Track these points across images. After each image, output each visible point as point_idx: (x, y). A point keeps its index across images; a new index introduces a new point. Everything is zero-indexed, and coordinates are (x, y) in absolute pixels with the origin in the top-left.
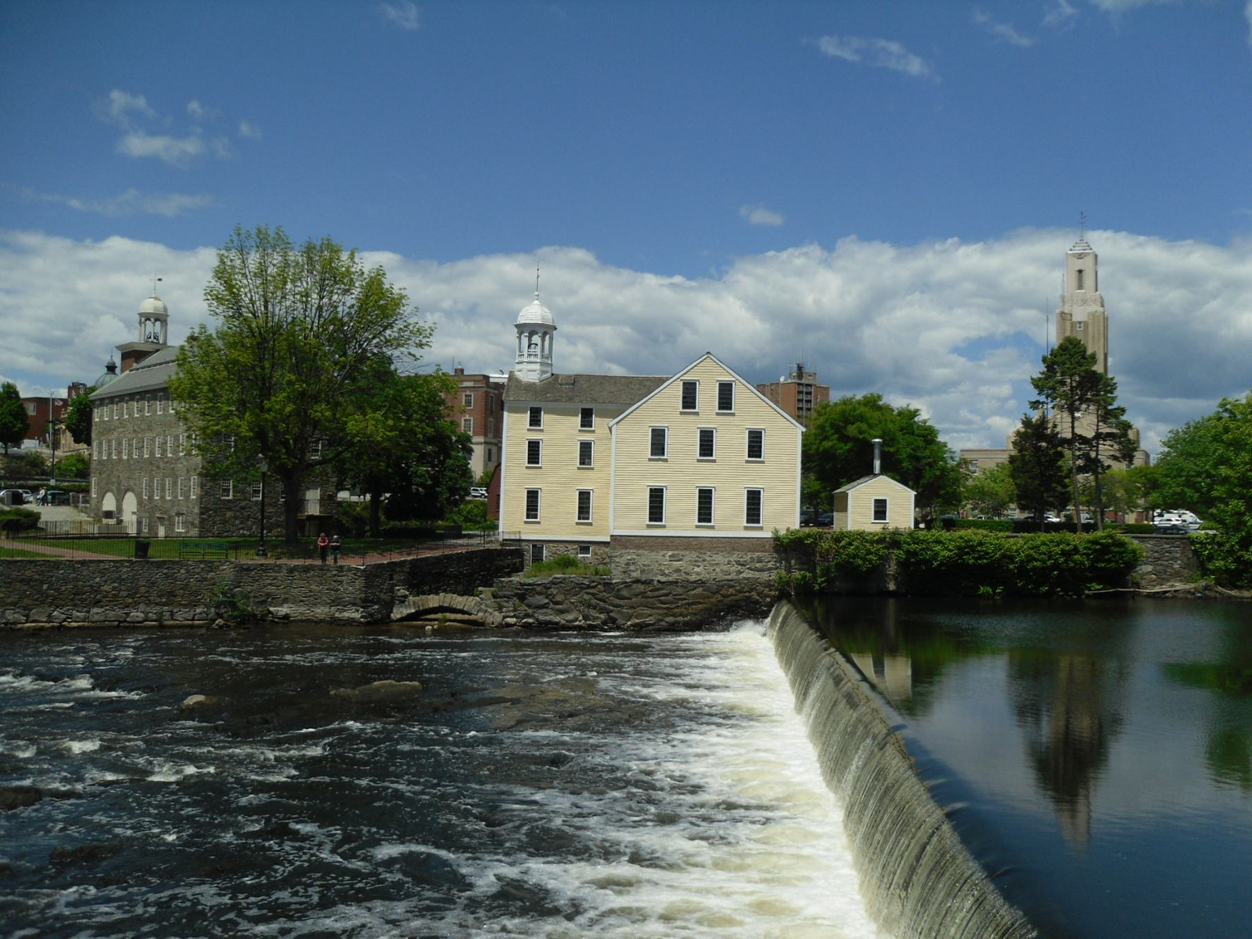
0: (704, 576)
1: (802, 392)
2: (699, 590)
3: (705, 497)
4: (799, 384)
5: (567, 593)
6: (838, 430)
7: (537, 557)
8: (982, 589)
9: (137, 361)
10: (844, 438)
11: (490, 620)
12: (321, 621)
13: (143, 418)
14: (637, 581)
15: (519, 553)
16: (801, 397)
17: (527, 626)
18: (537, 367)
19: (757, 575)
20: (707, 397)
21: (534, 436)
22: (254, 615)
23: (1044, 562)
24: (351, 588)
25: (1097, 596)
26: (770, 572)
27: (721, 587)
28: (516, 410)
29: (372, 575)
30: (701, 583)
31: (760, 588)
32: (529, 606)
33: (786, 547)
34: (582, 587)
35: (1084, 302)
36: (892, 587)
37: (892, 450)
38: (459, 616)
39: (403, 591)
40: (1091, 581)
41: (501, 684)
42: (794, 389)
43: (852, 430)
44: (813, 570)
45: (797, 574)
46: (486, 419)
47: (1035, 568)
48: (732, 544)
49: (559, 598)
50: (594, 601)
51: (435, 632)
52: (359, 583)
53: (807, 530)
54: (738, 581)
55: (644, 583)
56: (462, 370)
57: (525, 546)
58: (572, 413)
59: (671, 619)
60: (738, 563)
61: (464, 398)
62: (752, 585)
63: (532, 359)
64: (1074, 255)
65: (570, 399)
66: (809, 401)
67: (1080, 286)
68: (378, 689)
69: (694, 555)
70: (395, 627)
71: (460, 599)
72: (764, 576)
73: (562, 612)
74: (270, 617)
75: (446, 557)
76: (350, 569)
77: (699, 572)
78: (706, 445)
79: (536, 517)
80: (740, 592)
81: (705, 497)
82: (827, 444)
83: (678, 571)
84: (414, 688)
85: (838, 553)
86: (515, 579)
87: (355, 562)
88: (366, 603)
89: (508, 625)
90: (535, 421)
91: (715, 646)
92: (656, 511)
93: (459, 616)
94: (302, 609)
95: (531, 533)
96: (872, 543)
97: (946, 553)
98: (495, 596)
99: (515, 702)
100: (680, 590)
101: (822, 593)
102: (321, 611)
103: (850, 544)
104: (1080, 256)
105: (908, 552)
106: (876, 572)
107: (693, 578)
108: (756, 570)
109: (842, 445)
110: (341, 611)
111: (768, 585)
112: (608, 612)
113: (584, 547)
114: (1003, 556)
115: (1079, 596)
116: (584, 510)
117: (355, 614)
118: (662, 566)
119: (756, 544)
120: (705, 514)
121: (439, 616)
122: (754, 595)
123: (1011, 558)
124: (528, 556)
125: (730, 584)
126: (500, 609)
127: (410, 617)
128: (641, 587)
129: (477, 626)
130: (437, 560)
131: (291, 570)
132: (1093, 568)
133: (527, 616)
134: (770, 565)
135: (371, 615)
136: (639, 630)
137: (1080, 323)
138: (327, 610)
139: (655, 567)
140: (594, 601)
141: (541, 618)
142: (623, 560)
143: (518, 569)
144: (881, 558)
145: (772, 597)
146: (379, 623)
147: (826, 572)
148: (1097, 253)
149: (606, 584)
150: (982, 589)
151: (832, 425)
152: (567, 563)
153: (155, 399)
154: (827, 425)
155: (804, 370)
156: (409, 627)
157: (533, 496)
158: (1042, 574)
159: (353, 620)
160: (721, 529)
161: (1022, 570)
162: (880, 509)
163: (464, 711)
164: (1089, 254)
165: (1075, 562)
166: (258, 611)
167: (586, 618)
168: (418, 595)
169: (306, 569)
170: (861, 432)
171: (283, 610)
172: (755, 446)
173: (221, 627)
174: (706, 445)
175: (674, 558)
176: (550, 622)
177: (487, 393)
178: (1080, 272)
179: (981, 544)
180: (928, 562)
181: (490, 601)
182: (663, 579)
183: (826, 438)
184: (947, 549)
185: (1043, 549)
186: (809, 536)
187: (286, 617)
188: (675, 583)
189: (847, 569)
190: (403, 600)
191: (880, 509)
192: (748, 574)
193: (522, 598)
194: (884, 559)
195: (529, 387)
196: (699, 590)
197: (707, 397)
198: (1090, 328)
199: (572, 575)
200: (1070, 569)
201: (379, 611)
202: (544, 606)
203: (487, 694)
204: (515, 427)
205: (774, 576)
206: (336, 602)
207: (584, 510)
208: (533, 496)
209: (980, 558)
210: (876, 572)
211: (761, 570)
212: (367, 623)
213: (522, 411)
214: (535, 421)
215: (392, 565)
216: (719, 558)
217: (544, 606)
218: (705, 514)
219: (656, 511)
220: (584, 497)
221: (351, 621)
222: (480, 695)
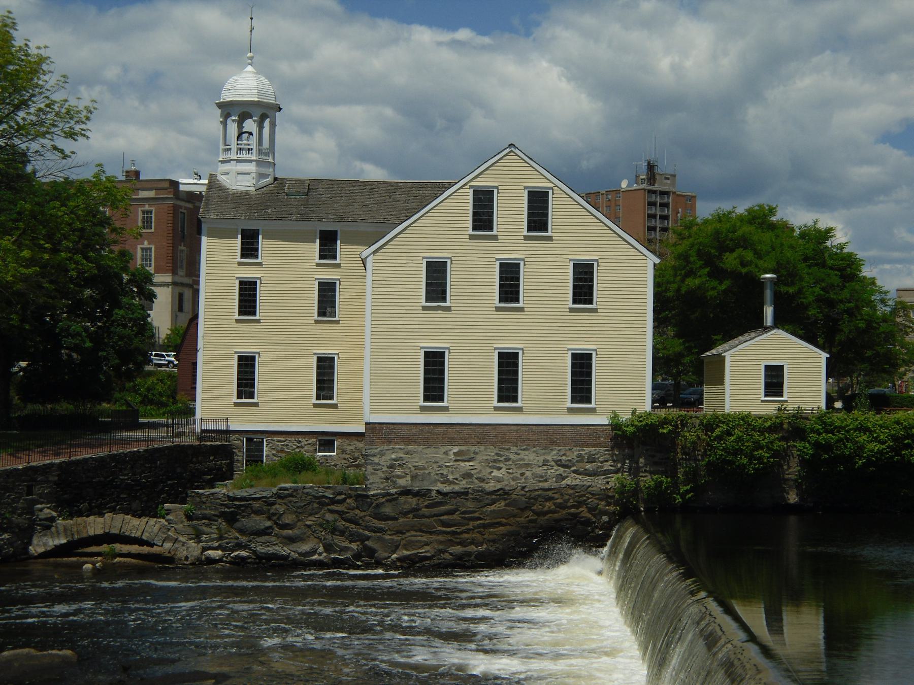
0: (509, 483)
7: (255, 457)
10: (718, 273)
11: (182, 553)
14: (406, 492)
15: (227, 452)
18: (252, 168)
19: (587, 480)
21: (249, 273)
28: (218, 233)
30: (502, 494)
31: (593, 501)
32: (242, 532)
34: (322, 502)
36: (793, 498)
38: (135, 549)
43: (730, 260)
44: (673, 474)
45: (647, 480)
46: (174, 247)
50: (341, 524)
51: (98, 573)
53: (662, 413)
54: (558, 490)
55: (417, 494)
56: (137, 173)
57: (234, 440)
59: (458, 549)
62: (581, 496)
63: (245, 155)
65: (304, 218)
69: (489, 452)
71: (135, 522)
72: (599, 483)
73: (292, 540)
75: (113, 457)
80: (562, 506)
82: (692, 283)
83: (467, 475)
86: (222, 490)
89: (211, 561)
90: (249, 250)
93: (135, 549)
96: (762, 431)
98: (189, 518)
100: (470, 505)
103: (729, 433)
105: (817, 445)
107: (491, 486)
108: (587, 473)
109: (714, 283)
111: (605, 496)
112: (362, 539)
113: (326, 440)
121: (104, 548)
122: (584, 512)
124: (241, 456)
125: (546, 495)
127: (59, 551)
128: (413, 502)
133: (239, 546)
134: (607, 466)
139: (433, 470)
140: (341, 524)
141: (261, 549)
142: (384, 461)
143: (226, 475)
144: (776, 454)
147: (692, 477)
151: (699, 254)
152: (300, 466)
154: (693, 253)
156: (57, 566)
157: (247, 364)
167: (328, 548)
168: (71, 516)
170: (743, 264)
176: (275, 556)
177: (175, 208)
180: (848, 460)
182: (446, 488)
183: (691, 273)
186: (665, 421)
188: (464, 494)
190: (47, 525)
193: (231, 519)
194: (781, 456)
199: (308, 483)
201: (10, 543)
202: (265, 532)
205: (613, 481)
208: (247, 364)
213: (231, 235)
214: (249, 250)
215: (31, 471)
216: (530, 456)
217: (265, 532)
220: (325, 366)
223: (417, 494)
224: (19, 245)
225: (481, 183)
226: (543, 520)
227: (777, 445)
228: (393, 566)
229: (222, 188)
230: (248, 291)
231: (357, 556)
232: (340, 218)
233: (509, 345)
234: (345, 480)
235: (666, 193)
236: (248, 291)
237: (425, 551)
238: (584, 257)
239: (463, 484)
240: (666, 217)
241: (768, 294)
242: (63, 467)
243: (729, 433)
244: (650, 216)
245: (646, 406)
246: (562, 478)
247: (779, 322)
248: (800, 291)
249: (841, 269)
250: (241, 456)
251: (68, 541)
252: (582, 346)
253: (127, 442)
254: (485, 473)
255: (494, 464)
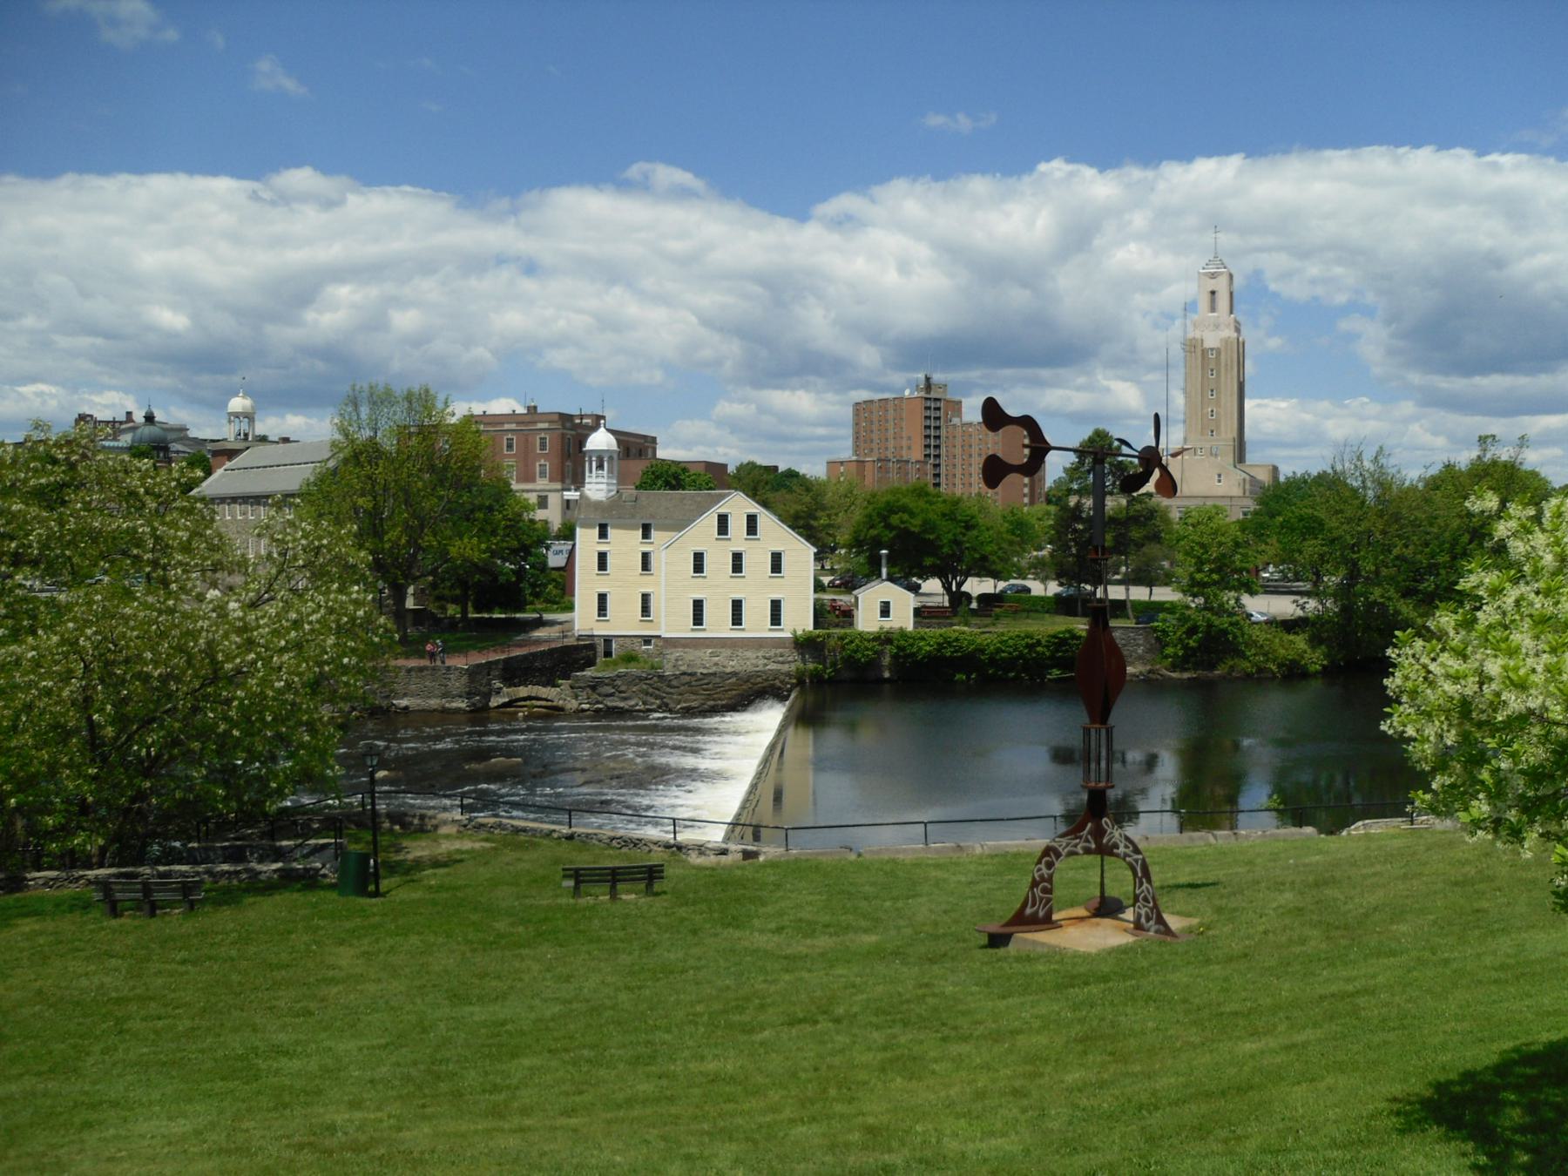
0: (737, 669)
1: (929, 408)
2: (734, 680)
3: (737, 606)
4: (926, 399)
5: (630, 684)
6: (885, 519)
7: (608, 654)
8: (958, 677)
9: (230, 459)
10: (889, 527)
11: (568, 706)
12: (435, 710)
13: (246, 521)
14: (684, 674)
15: (592, 647)
16: (928, 414)
17: (597, 711)
18: (604, 487)
19: (779, 667)
20: (737, 525)
21: (603, 548)
22: (381, 707)
23: (1010, 653)
24: (458, 684)
25: (1058, 680)
26: (792, 663)
27: (748, 678)
28: (586, 525)
29: (474, 672)
30: (734, 674)
31: (782, 677)
32: (599, 695)
33: (804, 645)
34: (641, 679)
35: (1217, 326)
36: (887, 675)
37: (932, 537)
38: (544, 703)
39: (497, 684)
40: (1053, 667)
41: (576, 759)
42: (921, 405)
43: (895, 520)
44: (823, 662)
45: (811, 666)
46: (563, 463)
47: (1002, 658)
48: (758, 643)
49: (623, 688)
50: (651, 690)
51: (526, 718)
52: (465, 679)
53: (817, 631)
54: (764, 672)
55: (690, 674)
56: (535, 408)
57: (596, 640)
58: (632, 527)
59: (712, 703)
60: (765, 658)
61: (538, 441)
62: (776, 675)
63: (600, 480)
64: (1205, 274)
65: (633, 516)
66: (938, 418)
67: (1213, 309)
68: (495, 764)
69: (729, 652)
70: (493, 714)
71: (544, 690)
72: (785, 668)
73: (625, 699)
74: (393, 709)
75: (531, 654)
76: (456, 669)
77: (732, 665)
78: (737, 562)
79: (605, 615)
80: (766, 680)
81: (737, 606)
82: (873, 532)
83: (716, 664)
84: (518, 764)
85: (843, 648)
86: (589, 673)
87: (460, 662)
88: (469, 695)
89: (583, 710)
90: (603, 534)
91: (731, 725)
92: (698, 619)
93: (544, 703)
94: (419, 701)
95: (602, 630)
96: (869, 641)
97: (928, 648)
98: (572, 687)
99: (583, 770)
100: (718, 680)
101: (831, 681)
102: (434, 703)
103: (852, 642)
104: (1213, 276)
105: (898, 647)
106: (874, 664)
107: (729, 670)
108: (779, 662)
109: (887, 532)
110: (450, 702)
111: (788, 674)
112: (662, 698)
113: (647, 640)
114: (976, 650)
115: (1043, 680)
116: (646, 610)
117: (462, 704)
118: (704, 661)
119: (778, 642)
120: (737, 619)
121: (528, 703)
122: (777, 683)
123: (982, 651)
124: (601, 649)
125: (757, 674)
126: (576, 697)
127: (504, 705)
128: (687, 678)
129: (556, 712)
130: (525, 657)
131: (409, 671)
132: (1052, 657)
133: (598, 702)
134: (790, 659)
135: (474, 704)
136: (689, 712)
137: (1212, 349)
138: (438, 701)
139: (698, 662)
140: (651, 690)
141: (609, 704)
142: (673, 657)
143: (591, 662)
144: (875, 653)
145: (792, 684)
146: (479, 714)
147: (834, 664)
148: (1233, 272)
149: (659, 676)
150: (958, 677)
151: (879, 514)
152: (630, 658)
153: (259, 504)
154: (874, 514)
155: (932, 381)
156: (504, 713)
157: (602, 598)
158: (1010, 663)
159: (460, 709)
160: (751, 631)
161: (992, 661)
162: (885, 610)
163: (1497, 583)
164: (1222, 273)
165: (1038, 653)
166: (384, 703)
167: (644, 703)
168: (510, 686)
169: (421, 669)
170: (902, 522)
171: (404, 702)
172: (776, 563)
173: (357, 718)
174: (737, 562)
175: (713, 655)
176: (616, 707)
177: (563, 435)
178: (1213, 293)
179: (957, 640)
180: (913, 655)
181: (569, 691)
182: (705, 671)
183: (872, 527)
184: (929, 645)
185: (1011, 642)
186: (818, 636)
187: (406, 708)
188: (714, 674)
189: (850, 662)
190: (498, 692)
191: (885, 610)
192: (772, 666)
193: (594, 688)
194: (880, 654)
195: (597, 505)
196: (734, 680)
197: (737, 525)
198: (1223, 357)
199: (633, 669)
200: (1033, 659)
201: (479, 701)
202: (612, 695)
203: (566, 766)
204: (586, 539)
205: (793, 667)
206: (444, 695)
207: (646, 610)
208: (602, 598)
209: (956, 651)
210: (874, 664)
211: (783, 663)
212: (471, 711)
213: (592, 527)
214: (603, 534)
215: (489, 663)
216: (749, 654)
217: (612, 695)
218: (737, 619)
219: (698, 619)
220: (645, 598)
221: (458, 711)
222: (562, 766)
223: (690, 674)
224: (480, 542)
225: (722, 511)
226: (756, 687)
227: (878, 648)
228: (677, 712)
229: (587, 499)
230: (602, 557)
231: (660, 707)
232: (652, 517)
233: (737, 596)
234: (653, 667)
235: (939, 400)
236: (602, 557)
237: (694, 704)
238: (777, 549)
239: (714, 669)
240: (939, 418)
241: (884, 561)
242: (506, 661)
243: (852, 642)
244: (926, 417)
245: (810, 627)
246: (766, 665)
247: (891, 579)
248: (938, 538)
249: (966, 522)
250: (601, 649)
251: (283, 417)
252: (776, 596)
253: (538, 642)
254: (725, 663)
255: (730, 658)
